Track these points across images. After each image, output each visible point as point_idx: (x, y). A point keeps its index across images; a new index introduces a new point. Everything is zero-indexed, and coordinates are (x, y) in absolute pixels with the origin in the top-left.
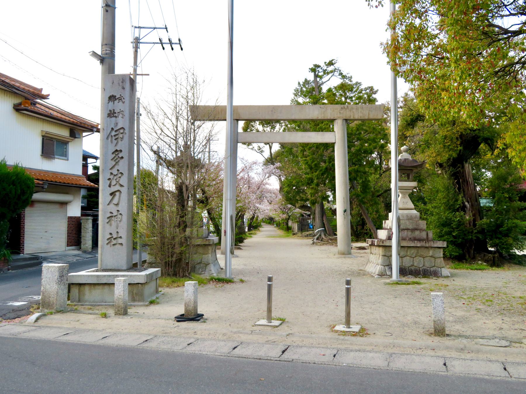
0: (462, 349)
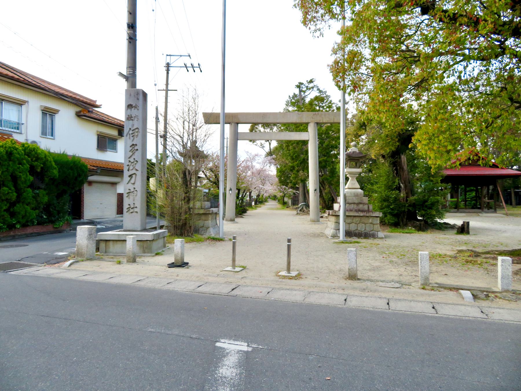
0: (364, 289)
